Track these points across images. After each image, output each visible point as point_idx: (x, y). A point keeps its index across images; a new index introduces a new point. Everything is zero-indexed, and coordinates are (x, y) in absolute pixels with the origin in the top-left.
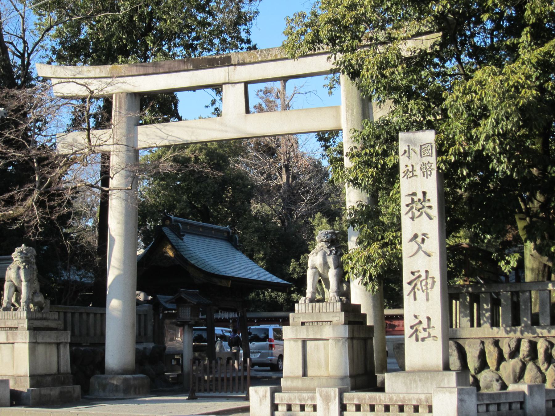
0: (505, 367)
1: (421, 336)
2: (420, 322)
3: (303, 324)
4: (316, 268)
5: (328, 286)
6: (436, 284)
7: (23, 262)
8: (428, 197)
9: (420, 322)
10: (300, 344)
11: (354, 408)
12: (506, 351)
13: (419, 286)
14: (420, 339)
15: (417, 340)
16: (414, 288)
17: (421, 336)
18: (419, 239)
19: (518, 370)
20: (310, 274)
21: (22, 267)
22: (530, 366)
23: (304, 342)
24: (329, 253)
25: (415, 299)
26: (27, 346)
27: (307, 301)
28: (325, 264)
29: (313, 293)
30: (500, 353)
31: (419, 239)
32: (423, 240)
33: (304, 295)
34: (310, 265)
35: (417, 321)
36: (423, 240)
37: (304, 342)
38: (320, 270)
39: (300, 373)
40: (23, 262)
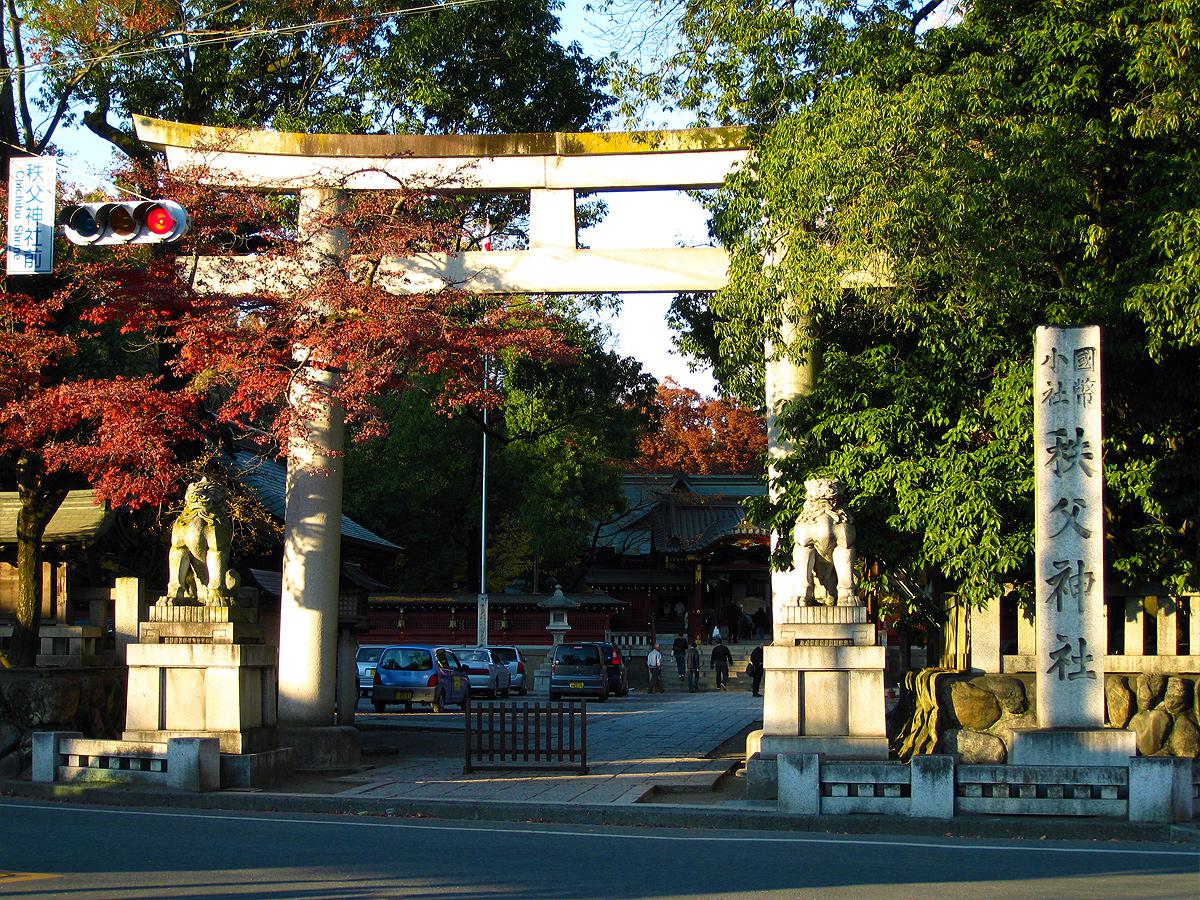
0: (1139, 723)
1: (1068, 670)
2: (1068, 647)
3: (798, 642)
4: (185, 547)
5: (205, 581)
6: (1095, 584)
7: (209, 512)
8: (1085, 438)
9: (1068, 647)
10: (795, 676)
11: (979, 792)
12: (1143, 694)
13: (1066, 585)
14: (1066, 676)
15: (1061, 677)
16: (1057, 590)
17: (1068, 670)
18: (1069, 508)
19: (1163, 728)
20: (175, 557)
21: (210, 522)
22: (1180, 721)
23: (801, 673)
24: (837, 519)
25: (1059, 608)
26: (236, 673)
27: (170, 603)
28: (203, 545)
29: (181, 590)
30: (1133, 697)
31: (1069, 508)
32: (1076, 509)
33: (164, 592)
34: (174, 540)
35: (1063, 645)
36: (1076, 509)
37: (801, 673)
38: (820, 549)
39: (155, 725)
40: (209, 512)
